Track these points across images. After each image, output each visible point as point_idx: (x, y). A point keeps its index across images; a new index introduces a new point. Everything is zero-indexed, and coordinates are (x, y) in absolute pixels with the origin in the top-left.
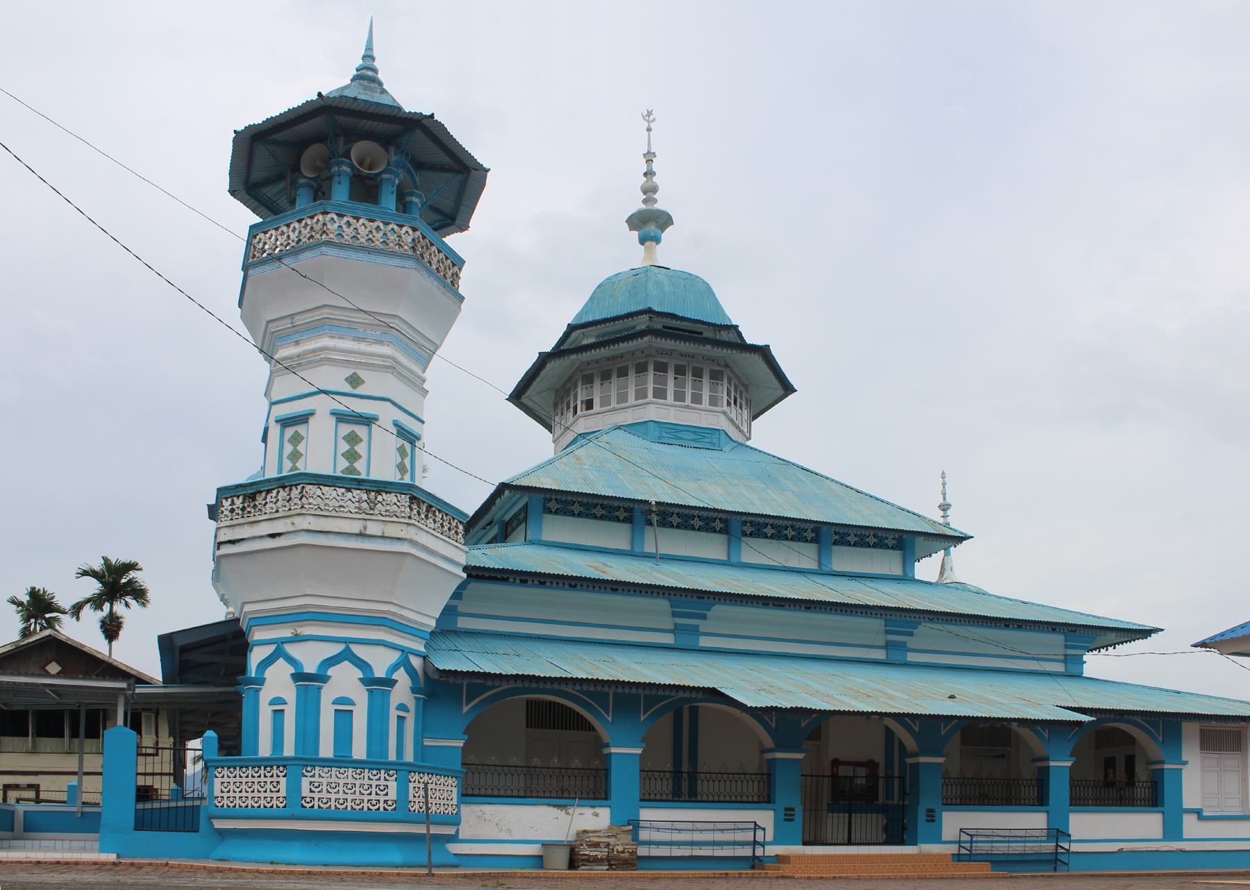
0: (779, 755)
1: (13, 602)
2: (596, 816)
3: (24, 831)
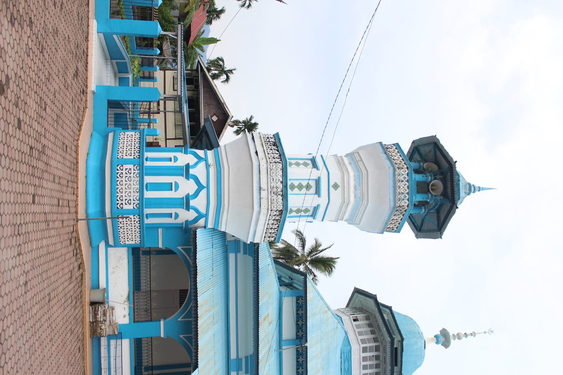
1: (251, 117)
3: (119, 78)
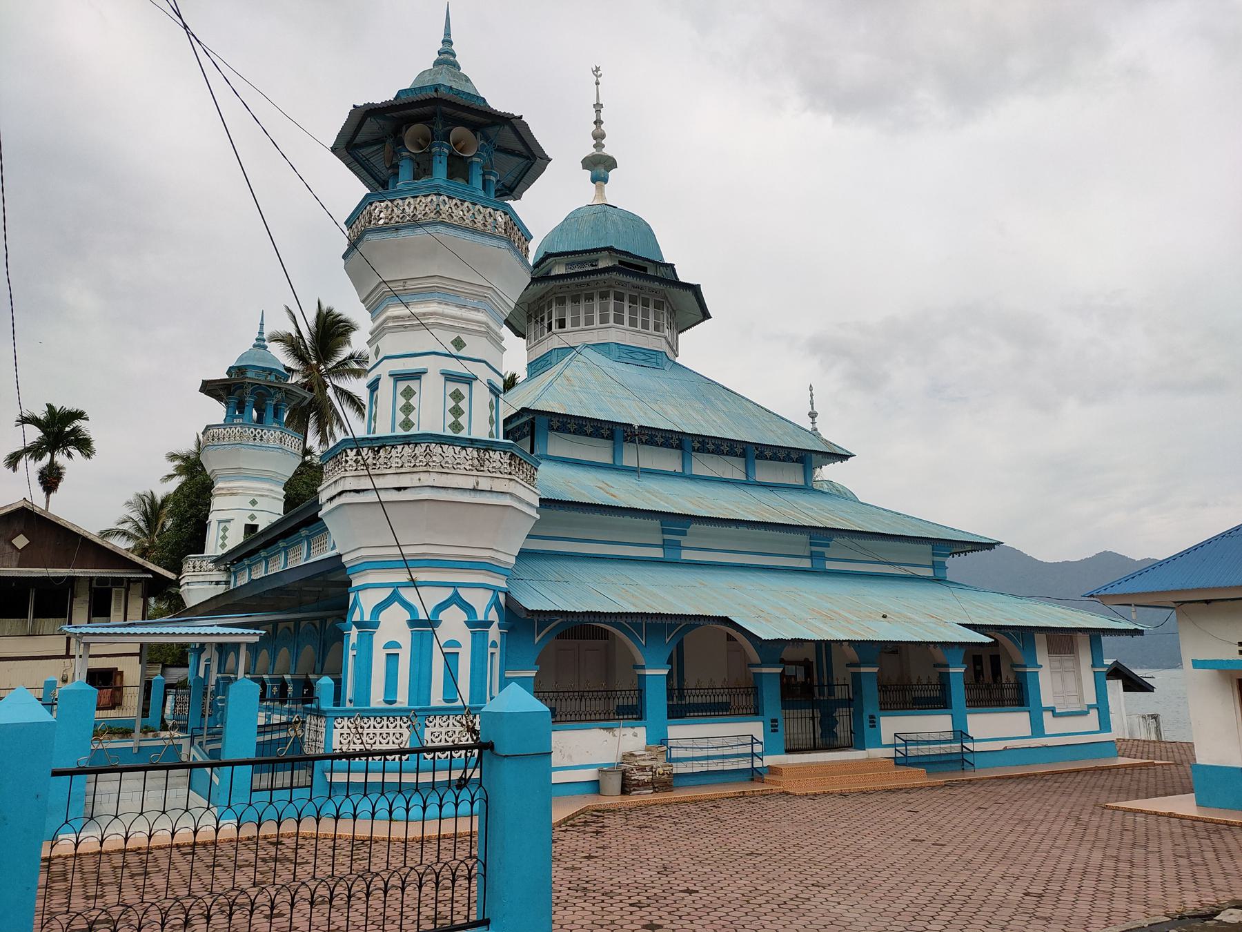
0: (765, 670)
2: (635, 736)
